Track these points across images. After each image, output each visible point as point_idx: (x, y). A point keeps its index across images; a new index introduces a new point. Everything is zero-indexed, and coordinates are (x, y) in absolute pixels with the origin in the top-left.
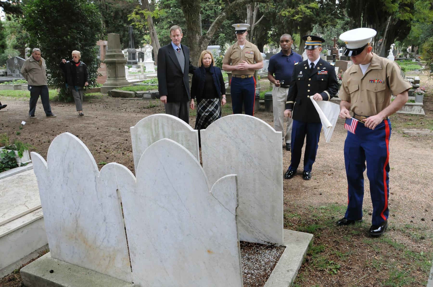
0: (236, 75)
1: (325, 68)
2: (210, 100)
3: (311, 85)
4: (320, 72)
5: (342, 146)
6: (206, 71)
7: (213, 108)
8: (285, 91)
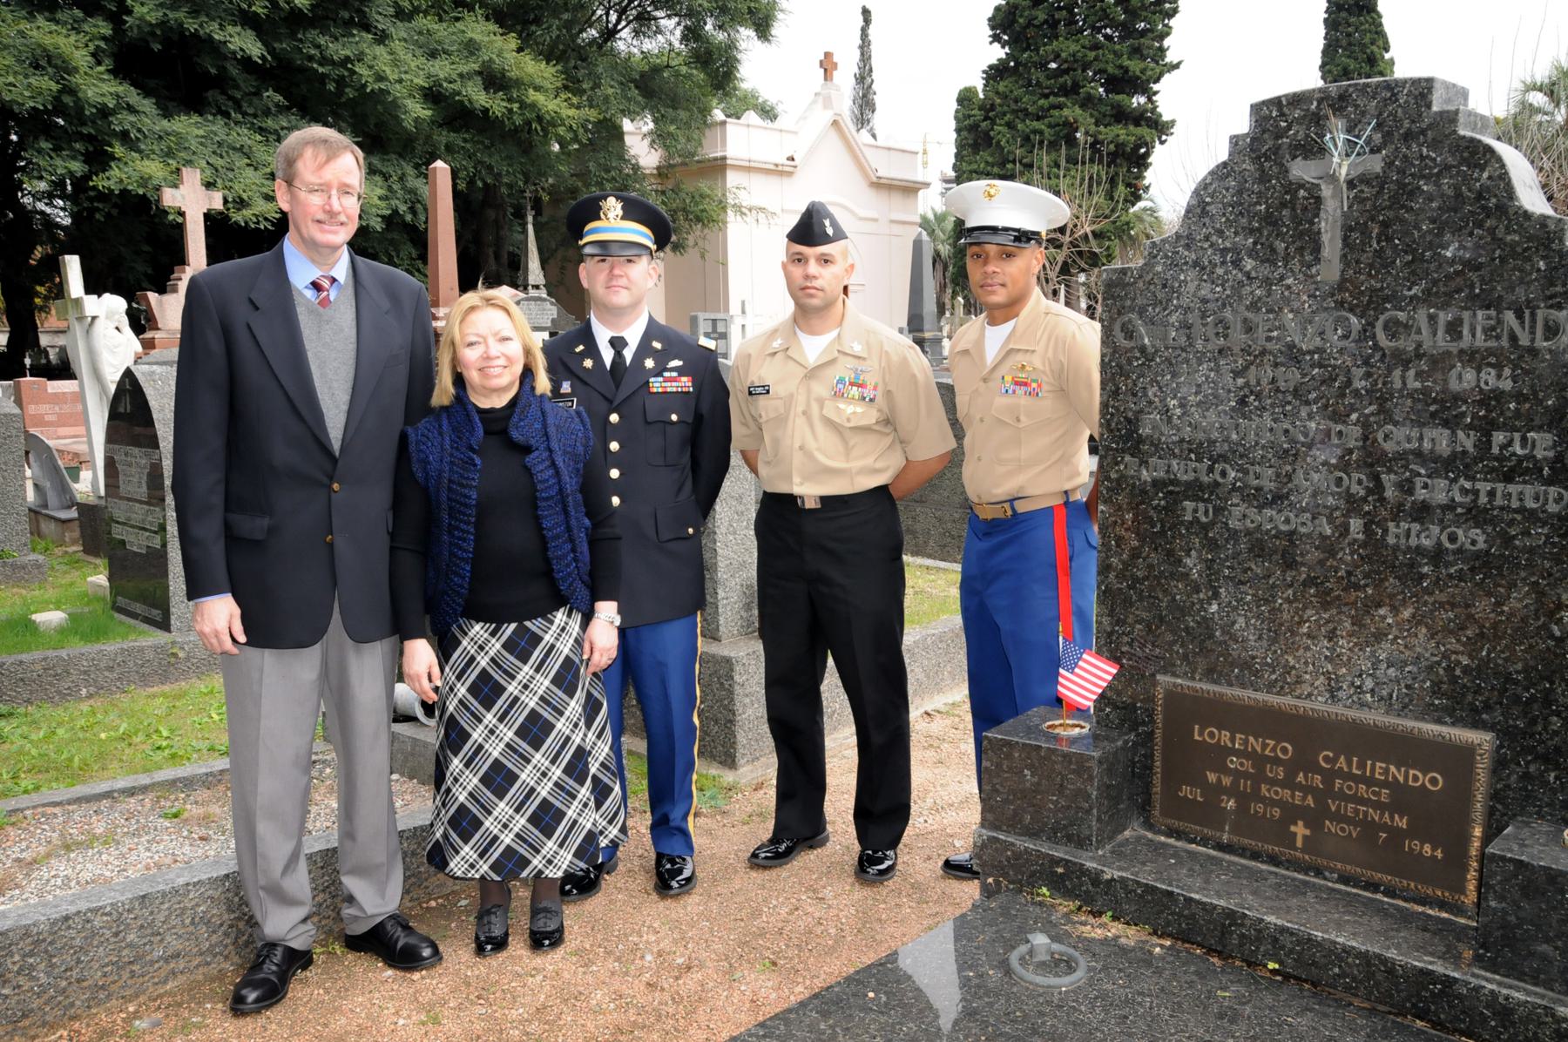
1: (676, 363)
2: (522, 630)
3: (621, 446)
4: (660, 379)
6: (486, 433)
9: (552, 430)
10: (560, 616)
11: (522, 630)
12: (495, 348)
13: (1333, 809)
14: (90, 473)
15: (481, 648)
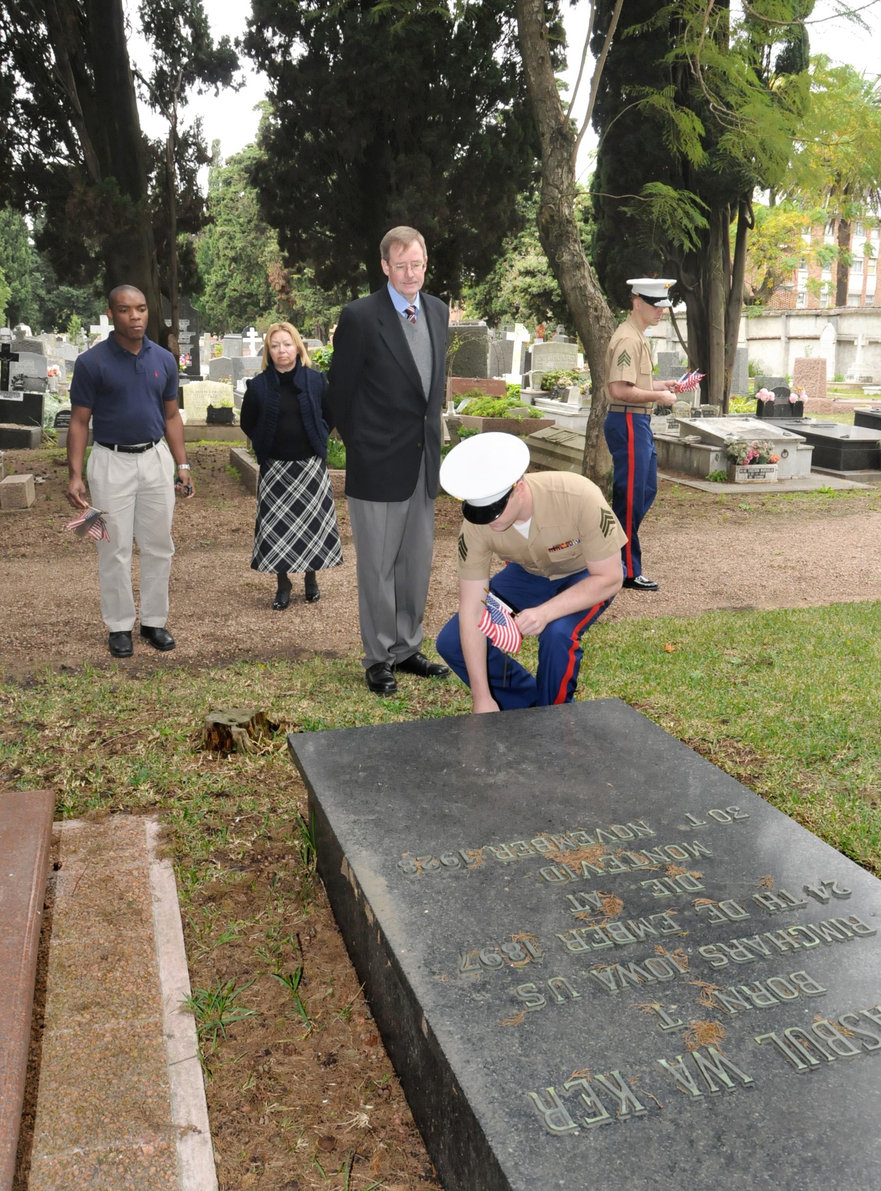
0: (626, 407)
5: (55, 1067)
7: (271, 529)
8: (133, 464)
9: (309, 383)
10: (311, 461)
11: (295, 465)
12: (283, 348)
13: (598, 830)
14: (238, 389)
15: (278, 471)
